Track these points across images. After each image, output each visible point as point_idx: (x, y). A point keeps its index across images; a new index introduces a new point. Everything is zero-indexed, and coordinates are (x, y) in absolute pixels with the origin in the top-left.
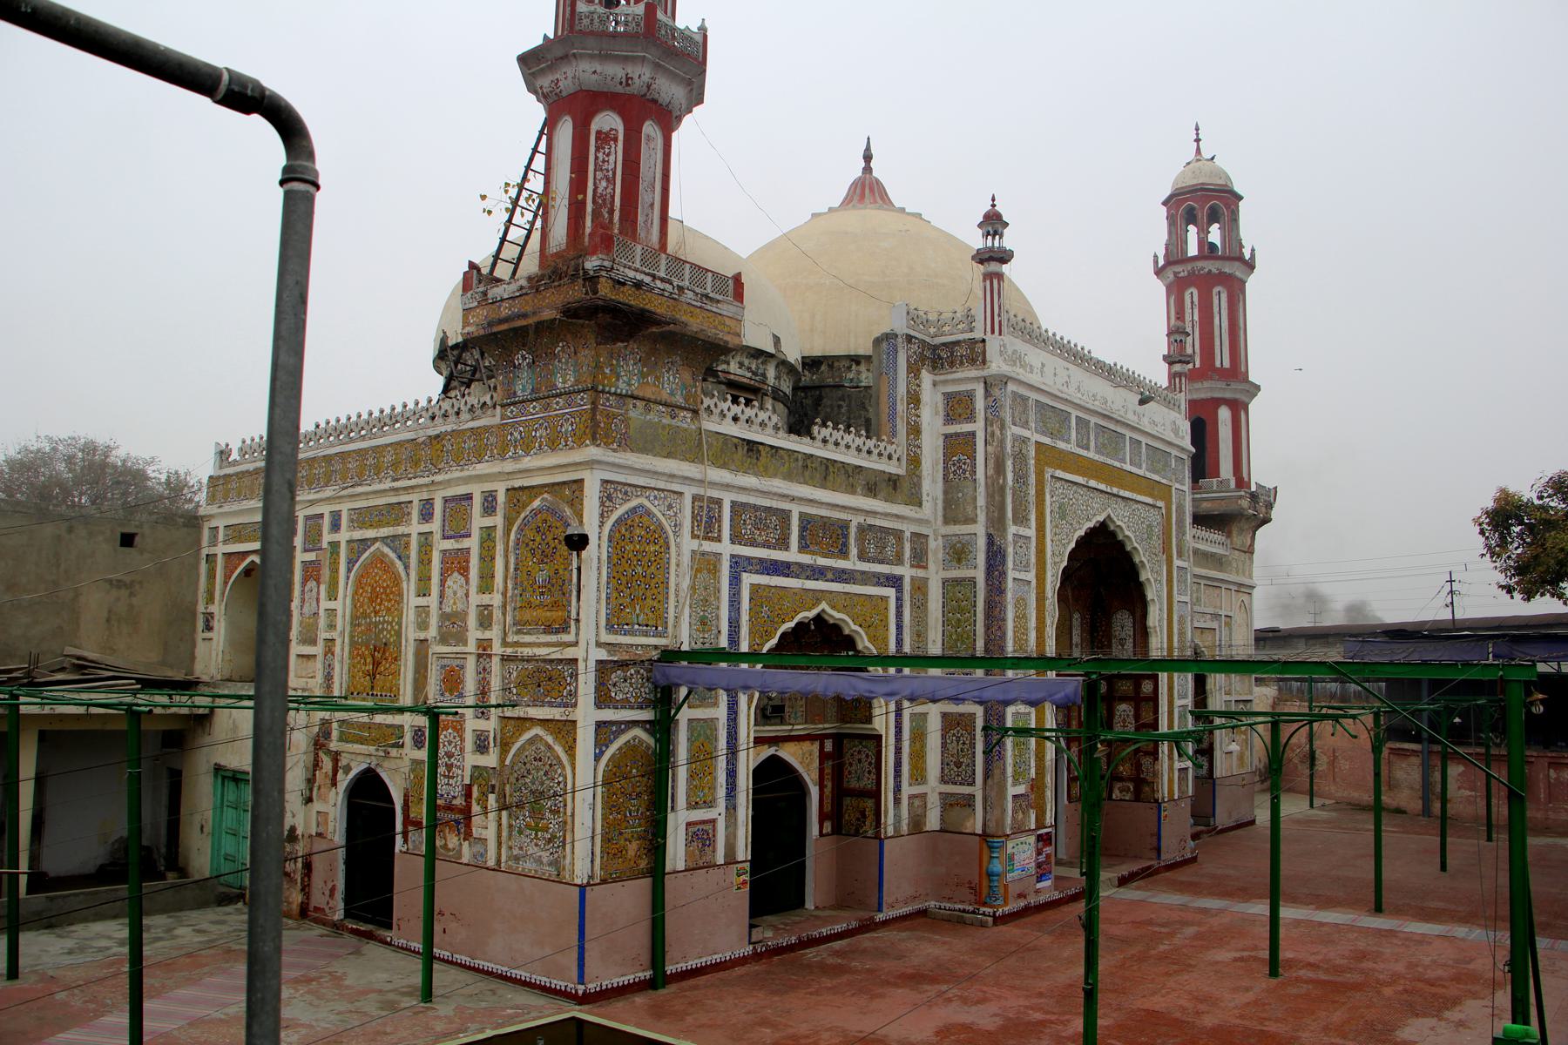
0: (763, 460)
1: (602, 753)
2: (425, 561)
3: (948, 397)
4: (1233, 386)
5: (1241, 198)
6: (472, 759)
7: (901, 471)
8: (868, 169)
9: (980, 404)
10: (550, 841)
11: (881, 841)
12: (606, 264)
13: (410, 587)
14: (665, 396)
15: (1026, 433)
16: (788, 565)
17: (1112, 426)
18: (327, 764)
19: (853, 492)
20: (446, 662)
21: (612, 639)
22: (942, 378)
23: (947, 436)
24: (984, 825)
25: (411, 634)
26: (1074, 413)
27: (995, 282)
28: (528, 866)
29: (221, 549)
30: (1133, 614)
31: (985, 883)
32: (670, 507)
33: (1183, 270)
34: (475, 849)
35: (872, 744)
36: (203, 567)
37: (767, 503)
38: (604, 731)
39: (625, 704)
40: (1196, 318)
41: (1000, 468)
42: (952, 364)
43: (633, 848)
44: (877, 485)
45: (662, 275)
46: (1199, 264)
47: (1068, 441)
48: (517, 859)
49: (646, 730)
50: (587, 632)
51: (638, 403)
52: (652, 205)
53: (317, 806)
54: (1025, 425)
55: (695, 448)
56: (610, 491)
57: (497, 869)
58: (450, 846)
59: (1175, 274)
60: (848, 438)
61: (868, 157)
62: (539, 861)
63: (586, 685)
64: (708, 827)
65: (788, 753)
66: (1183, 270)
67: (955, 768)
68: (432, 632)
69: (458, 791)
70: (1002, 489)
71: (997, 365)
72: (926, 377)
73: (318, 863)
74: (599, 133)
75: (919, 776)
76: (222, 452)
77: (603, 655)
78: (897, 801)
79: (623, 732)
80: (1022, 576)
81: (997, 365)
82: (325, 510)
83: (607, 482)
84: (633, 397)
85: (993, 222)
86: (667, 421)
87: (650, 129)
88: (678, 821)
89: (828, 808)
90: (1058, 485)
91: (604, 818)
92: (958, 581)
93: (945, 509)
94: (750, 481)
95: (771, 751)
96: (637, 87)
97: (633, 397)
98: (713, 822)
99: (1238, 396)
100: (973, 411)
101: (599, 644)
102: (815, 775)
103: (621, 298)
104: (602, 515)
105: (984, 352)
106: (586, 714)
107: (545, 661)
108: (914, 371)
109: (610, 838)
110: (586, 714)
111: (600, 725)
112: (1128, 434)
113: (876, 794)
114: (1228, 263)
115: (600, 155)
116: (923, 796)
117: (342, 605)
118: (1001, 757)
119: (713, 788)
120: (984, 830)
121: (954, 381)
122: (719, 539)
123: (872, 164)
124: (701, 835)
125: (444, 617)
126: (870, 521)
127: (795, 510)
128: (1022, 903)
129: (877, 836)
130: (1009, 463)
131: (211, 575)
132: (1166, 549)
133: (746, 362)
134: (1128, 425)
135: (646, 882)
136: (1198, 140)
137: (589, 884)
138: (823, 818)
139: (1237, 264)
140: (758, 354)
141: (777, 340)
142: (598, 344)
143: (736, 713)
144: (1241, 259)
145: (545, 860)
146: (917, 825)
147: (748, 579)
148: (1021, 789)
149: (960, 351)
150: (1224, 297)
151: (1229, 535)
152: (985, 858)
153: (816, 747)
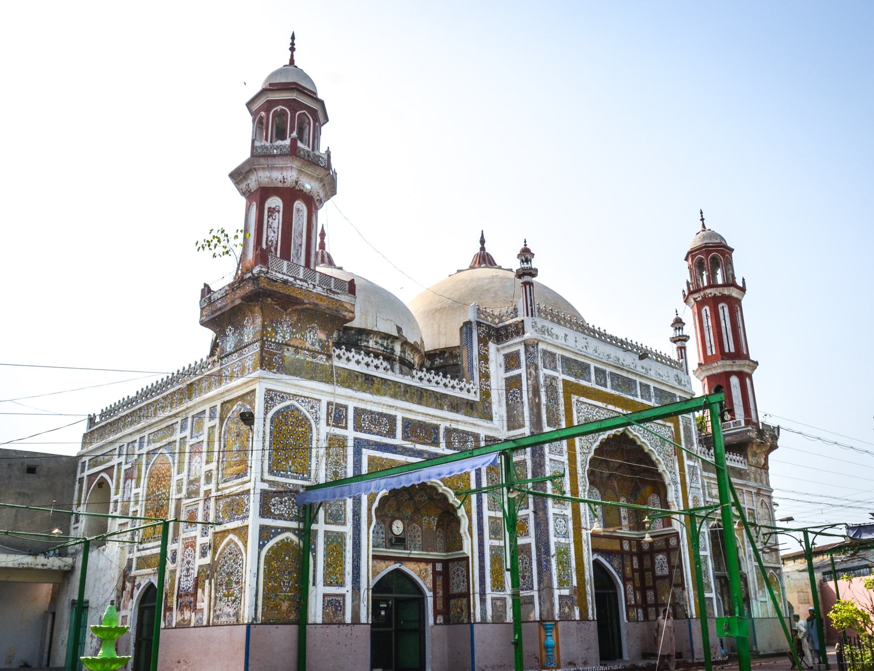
0: (376, 386)
1: (264, 545)
4: (738, 362)
5: (732, 250)
7: (477, 399)
8: (483, 249)
9: (523, 357)
10: (234, 601)
11: (472, 625)
12: (264, 269)
13: (174, 470)
14: (308, 345)
17: (624, 374)
18: (129, 585)
19: (442, 409)
20: (190, 508)
21: (272, 478)
22: (502, 346)
23: (507, 379)
24: (541, 614)
25: (174, 495)
26: (593, 365)
27: (528, 287)
28: (224, 619)
30: (659, 495)
31: (544, 653)
32: (312, 407)
33: (699, 296)
34: (198, 617)
35: (464, 563)
38: (265, 533)
39: (281, 517)
40: (710, 324)
41: (536, 392)
42: (507, 337)
43: (285, 605)
45: (301, 277)
46: (708, 291)
47: (589, 381)
49: (295, 534)
50: (254, 473)
51: (290, 348)
52: (301, 245)
53: (123, 613)
54: (555, 369)
55: (328, 376)
57: (208, 626)
58: (186, 618)
59: (695, 299)
60: (437, 378)
61: (482, 241)
62: (229, 615)
63: (254, 504)
64: (340, 599)
65: (409, 569)
66: (699, 296)
68: (184, 492)
69: (191, 583)
70: (538, 405)
72: (492, 346)
74: (269, 208)
77: (266, 486)
78: (483, 601)
79: (279, 533)
80: (557, 458)
82: (137, 437)
83: (270, 390)
84: (286, 345)
85: (526, 254)
86: (309, 359)
87: (299, 205)
88: (317, 593)
89: (440, 606)
90: (583, 406)
91: (265, 584)
93: (508, 421)
94: (367, 396)
95: (397, 566)
96: (289, 183)
97: (286, 345)
98: (343, 596)
99: (742, 369)
100: (519, 363)
101: (263, 480)
102: (430, 585)
103: (274, 288)
104: (267, 408)
105: (523, 328)
107: (235, 495)
108: (483, 342)
109: (270, 595)
110: (254, 521)
111: (263, 529)
112: (638, 380)
113: (467, 595)
114: (726, 289)
115: (270, 220)
117: (142, 491)
118: (549, 569)
119: (343, 575)
120: (541, 618)
121: (508, 346)
122: (346, 428)
123: (485, 246)
124: (333, 604)
125: (191, 483)
126: (454, 426)
127: (399, 416)
129: (469, 622)
130: (543, 390)
132: (678, 451)
133: (380, 341)
134: (637, 374)
136: (702, 220)
137: (252, 623)
138: (436, 613)
139: (732, 288)
140: (386, 336)
141: (399, 329)
143: (360, 531)
144: (734, 285)
145: (231, 614)
147: (366, 453)
148: (566, 592)
150: (726, 309)
151: (746, 457)
152: (543, 636)
153: (430, 567)
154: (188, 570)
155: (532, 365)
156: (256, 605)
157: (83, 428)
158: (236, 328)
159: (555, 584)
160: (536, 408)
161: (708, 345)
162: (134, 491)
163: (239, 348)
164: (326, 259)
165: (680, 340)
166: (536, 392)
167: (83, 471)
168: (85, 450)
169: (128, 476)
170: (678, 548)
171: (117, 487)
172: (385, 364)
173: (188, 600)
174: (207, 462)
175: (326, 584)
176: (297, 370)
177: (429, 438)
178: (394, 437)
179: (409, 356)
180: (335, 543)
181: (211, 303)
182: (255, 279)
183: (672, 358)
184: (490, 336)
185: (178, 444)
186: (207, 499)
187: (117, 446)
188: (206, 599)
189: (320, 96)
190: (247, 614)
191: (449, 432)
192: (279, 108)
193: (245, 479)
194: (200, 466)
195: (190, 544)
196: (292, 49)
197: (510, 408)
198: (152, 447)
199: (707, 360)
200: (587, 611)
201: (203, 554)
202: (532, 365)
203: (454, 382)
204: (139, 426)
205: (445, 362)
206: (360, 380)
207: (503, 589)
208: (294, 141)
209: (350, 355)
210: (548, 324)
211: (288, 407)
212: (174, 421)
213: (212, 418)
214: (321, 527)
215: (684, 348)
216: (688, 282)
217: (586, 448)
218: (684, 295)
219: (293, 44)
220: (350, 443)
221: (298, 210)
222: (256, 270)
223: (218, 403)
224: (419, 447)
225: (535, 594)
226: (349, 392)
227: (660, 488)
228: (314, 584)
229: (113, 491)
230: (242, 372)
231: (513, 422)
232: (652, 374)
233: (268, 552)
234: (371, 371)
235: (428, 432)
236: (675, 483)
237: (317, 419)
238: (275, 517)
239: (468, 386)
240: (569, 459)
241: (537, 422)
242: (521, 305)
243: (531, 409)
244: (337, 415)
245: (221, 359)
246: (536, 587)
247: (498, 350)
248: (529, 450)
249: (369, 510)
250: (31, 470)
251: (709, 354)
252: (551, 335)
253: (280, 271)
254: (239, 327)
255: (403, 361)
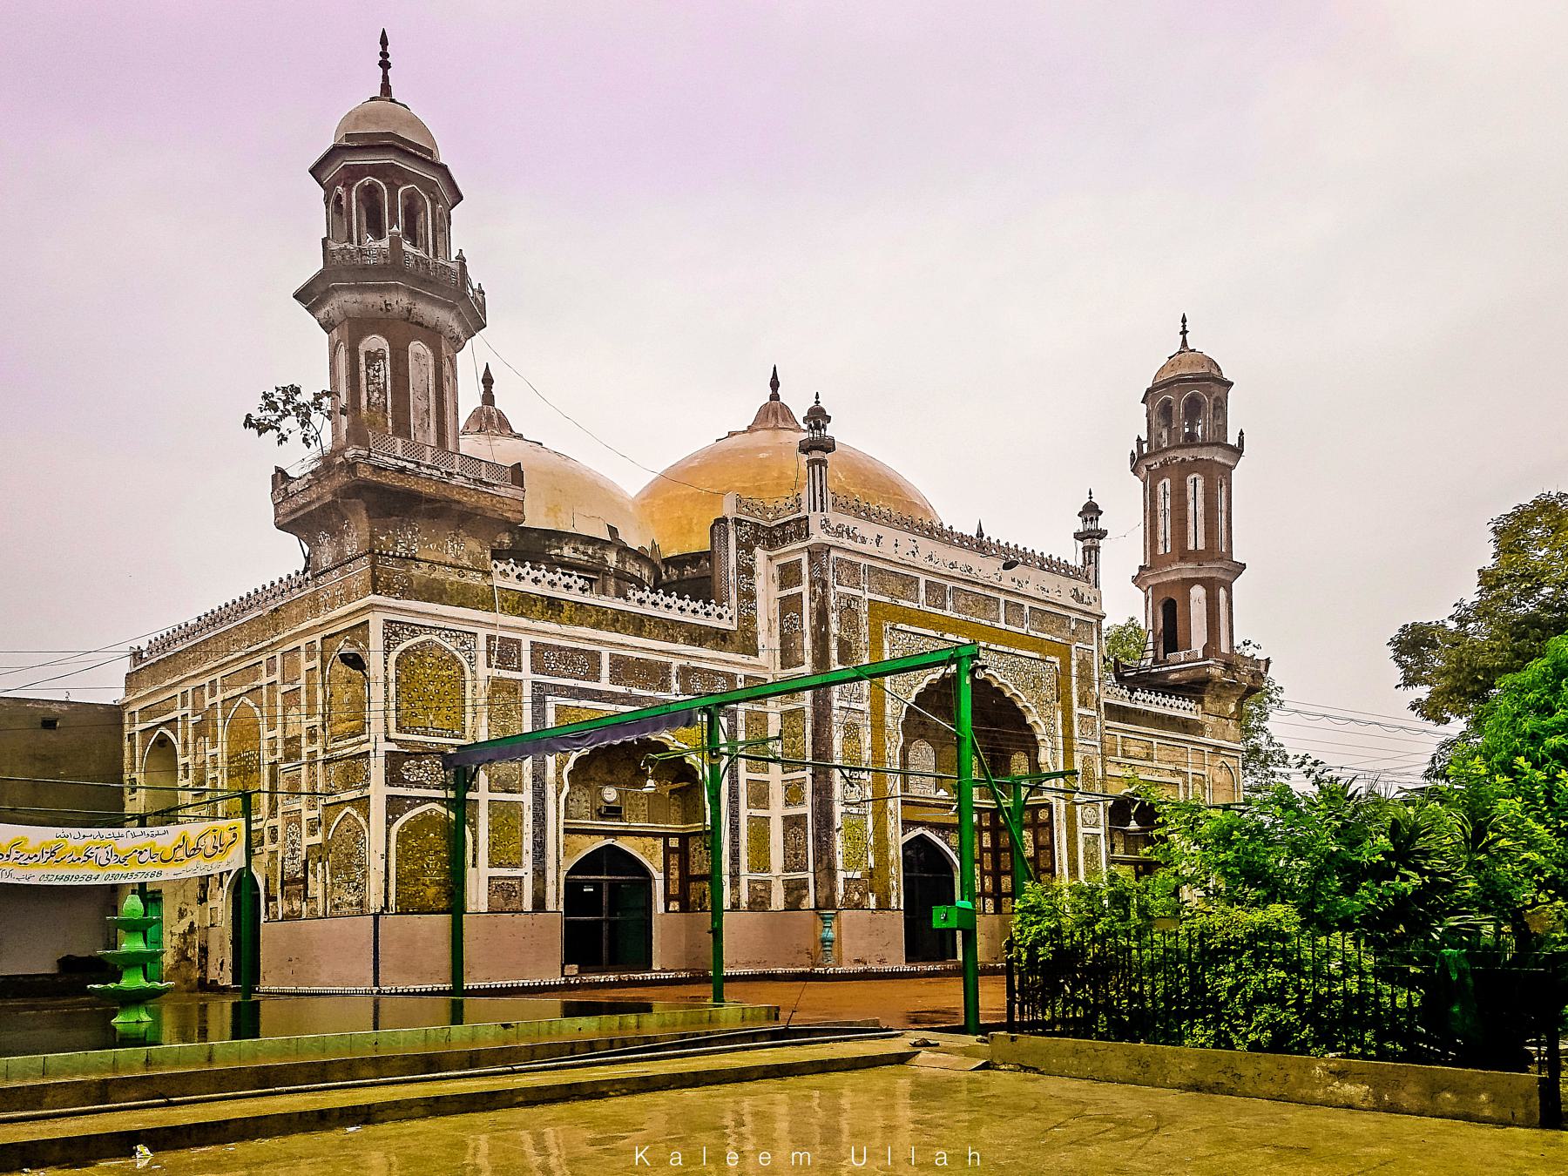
2: (272, 704)
3: (782, 567)
6: (308, 840)
8: (775, 397)
13: (263, 727)
15: (860, 593)
16: (599, 692)
17: (977, 590)
25: (267, 758)
28: (345, 909)
29: (139, 727)
36: (127, 743)
37: (574, 645)
38: (395, 806)
39: (419, 785)
41: (822, 616)
42: (784, 541)
43: (431, 892)
44: (720, 638)
46: (1172, 454)
48: (337, 906)
50: (376, 728)
52: (427, 411)
53: (211, 904)
56: (393, 631)
61: (775, 384)
63: (377, 769)
65: (623, 844)
67: (793, 861)
68: (280, 754)
71: (818, 536)
72: (760, 554)
73: (213, 947)
75: (761, 861)
76: (135, 654)
77: (393, 747)
78: (735, 884)
81: (818, 536)
82: (206, 681)
89: (674, 889)
92: (791, 713)
94: (552, 627)
95: (609, 841)
101: (388, 740)
106: (378, 791)
108: (746, 547)
110: (378, 791)
111: (391, 799)
116: (767, 884)
117: (221, 751)
122: (519, 669)
124: (504, 892)
125: (287, 742)
126: (694, 664)
128: (861, 968)
131: (133, 747)
132: (1063, 696)
133: (581, 548)
135: (446, 919)
138: (668, 899)
141: (613, 531)
142: (370, 517)
144: (1222, 444)
146: (759, 902)
147: (552, 702)
149: (790, 529)
150: (1200, 483)
151: (1200, 701)
154: (293, 851)
155: (820, 582)
156: (386, 890)
157: (126, 666)
158: (333, 535)
159: (839, 864)
160: (821, 640)
161: (1161, 538)
162: (210, 752)
163: (341, 563)
164: (496, 421)
165: (1091, 537)
166: (822, 616)
167: (133, 724)
168: (131, 698)
169: (200, 730)
170: (1049, 823)
171: (185, 744)
172: (581, 582)
173: (296, 885)
174: (308, 716)
175: (492, 865)
176: (434, 592)
177: (654, 680)
178: (598, 680)
179: (632, 568)
180: (505, 817)
181: (288, 497)
182: (351, 467)
183: (1071, 563)
184: (757, 539)
185: (264, 691)
186: (312, 763)
187: (178, 691)
188: (320, 887)
189: (442, 161)
190: (375, 902)
191: (685, 672)
192: (368, 180)
193: (363, 738)
194: (300, 723)
195: (294, 819)
196: (385, 65)
197: (785, 639)
198: (228, 695)
199: (1153, 563)
200: (888, 898)
201: (313, 832)
202: (820, 582)
203: (697, 605)
204: (206, 667)
205: (692, 577)
206: (539, 606)
207: (767, 869)
208: (395, 242)
209: (523, 572)
210: (848, 521)
211: (423, 643)
212: (257, 660)
213: (310, 658)
214: (482, 795)
215: (1097, 549)
216: (1139, 439)
217: (904, 691)
218: (1132, 460)
219: (384, 54)
220: (527, 690)
221: (417, 356)
222: (349, 453)
223: (317, 638)
224: (636, 691)
225: (810, 876)
226: (523, 622)
227: (1030, 745)
228: (474, 866)
229: (179, 749)
230: (348, 597)
231: (788, 656)
232: (1030, 590)
233: (402, 827)
234: (559, 593)
235: (655, 674)
236: (1052, 736)
237: (472, 660)
238: (409, 784)
239: (718, 610)
240: (872, 707)
241: (821, 660)
242: (805, 495)
243: (815, 642)
244: (505, 653)
245: (315, 577)
246: (811, 868)
247: (770, 559)
248: (808, 694)
249: (559, 774)
250: (49, 724)
251: (1161, 551)
252: (854, 538)
253: (393, 453)
254: (336, 533)
255: (622, 577)
